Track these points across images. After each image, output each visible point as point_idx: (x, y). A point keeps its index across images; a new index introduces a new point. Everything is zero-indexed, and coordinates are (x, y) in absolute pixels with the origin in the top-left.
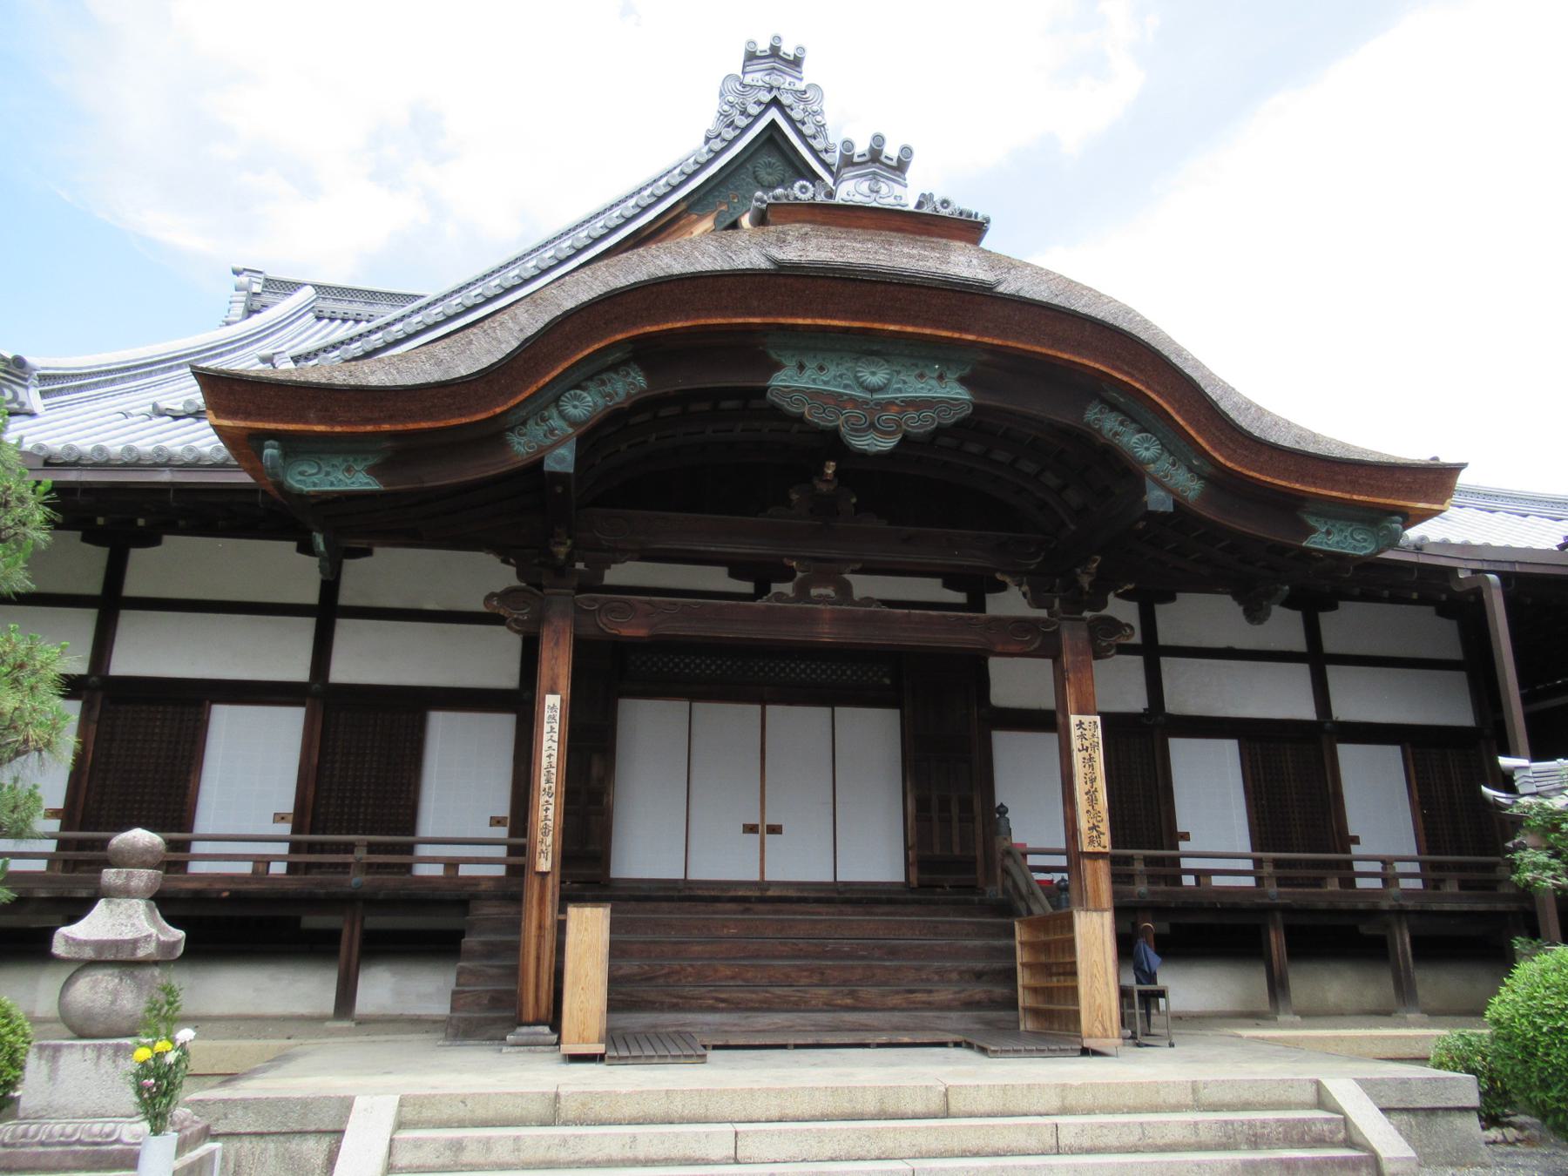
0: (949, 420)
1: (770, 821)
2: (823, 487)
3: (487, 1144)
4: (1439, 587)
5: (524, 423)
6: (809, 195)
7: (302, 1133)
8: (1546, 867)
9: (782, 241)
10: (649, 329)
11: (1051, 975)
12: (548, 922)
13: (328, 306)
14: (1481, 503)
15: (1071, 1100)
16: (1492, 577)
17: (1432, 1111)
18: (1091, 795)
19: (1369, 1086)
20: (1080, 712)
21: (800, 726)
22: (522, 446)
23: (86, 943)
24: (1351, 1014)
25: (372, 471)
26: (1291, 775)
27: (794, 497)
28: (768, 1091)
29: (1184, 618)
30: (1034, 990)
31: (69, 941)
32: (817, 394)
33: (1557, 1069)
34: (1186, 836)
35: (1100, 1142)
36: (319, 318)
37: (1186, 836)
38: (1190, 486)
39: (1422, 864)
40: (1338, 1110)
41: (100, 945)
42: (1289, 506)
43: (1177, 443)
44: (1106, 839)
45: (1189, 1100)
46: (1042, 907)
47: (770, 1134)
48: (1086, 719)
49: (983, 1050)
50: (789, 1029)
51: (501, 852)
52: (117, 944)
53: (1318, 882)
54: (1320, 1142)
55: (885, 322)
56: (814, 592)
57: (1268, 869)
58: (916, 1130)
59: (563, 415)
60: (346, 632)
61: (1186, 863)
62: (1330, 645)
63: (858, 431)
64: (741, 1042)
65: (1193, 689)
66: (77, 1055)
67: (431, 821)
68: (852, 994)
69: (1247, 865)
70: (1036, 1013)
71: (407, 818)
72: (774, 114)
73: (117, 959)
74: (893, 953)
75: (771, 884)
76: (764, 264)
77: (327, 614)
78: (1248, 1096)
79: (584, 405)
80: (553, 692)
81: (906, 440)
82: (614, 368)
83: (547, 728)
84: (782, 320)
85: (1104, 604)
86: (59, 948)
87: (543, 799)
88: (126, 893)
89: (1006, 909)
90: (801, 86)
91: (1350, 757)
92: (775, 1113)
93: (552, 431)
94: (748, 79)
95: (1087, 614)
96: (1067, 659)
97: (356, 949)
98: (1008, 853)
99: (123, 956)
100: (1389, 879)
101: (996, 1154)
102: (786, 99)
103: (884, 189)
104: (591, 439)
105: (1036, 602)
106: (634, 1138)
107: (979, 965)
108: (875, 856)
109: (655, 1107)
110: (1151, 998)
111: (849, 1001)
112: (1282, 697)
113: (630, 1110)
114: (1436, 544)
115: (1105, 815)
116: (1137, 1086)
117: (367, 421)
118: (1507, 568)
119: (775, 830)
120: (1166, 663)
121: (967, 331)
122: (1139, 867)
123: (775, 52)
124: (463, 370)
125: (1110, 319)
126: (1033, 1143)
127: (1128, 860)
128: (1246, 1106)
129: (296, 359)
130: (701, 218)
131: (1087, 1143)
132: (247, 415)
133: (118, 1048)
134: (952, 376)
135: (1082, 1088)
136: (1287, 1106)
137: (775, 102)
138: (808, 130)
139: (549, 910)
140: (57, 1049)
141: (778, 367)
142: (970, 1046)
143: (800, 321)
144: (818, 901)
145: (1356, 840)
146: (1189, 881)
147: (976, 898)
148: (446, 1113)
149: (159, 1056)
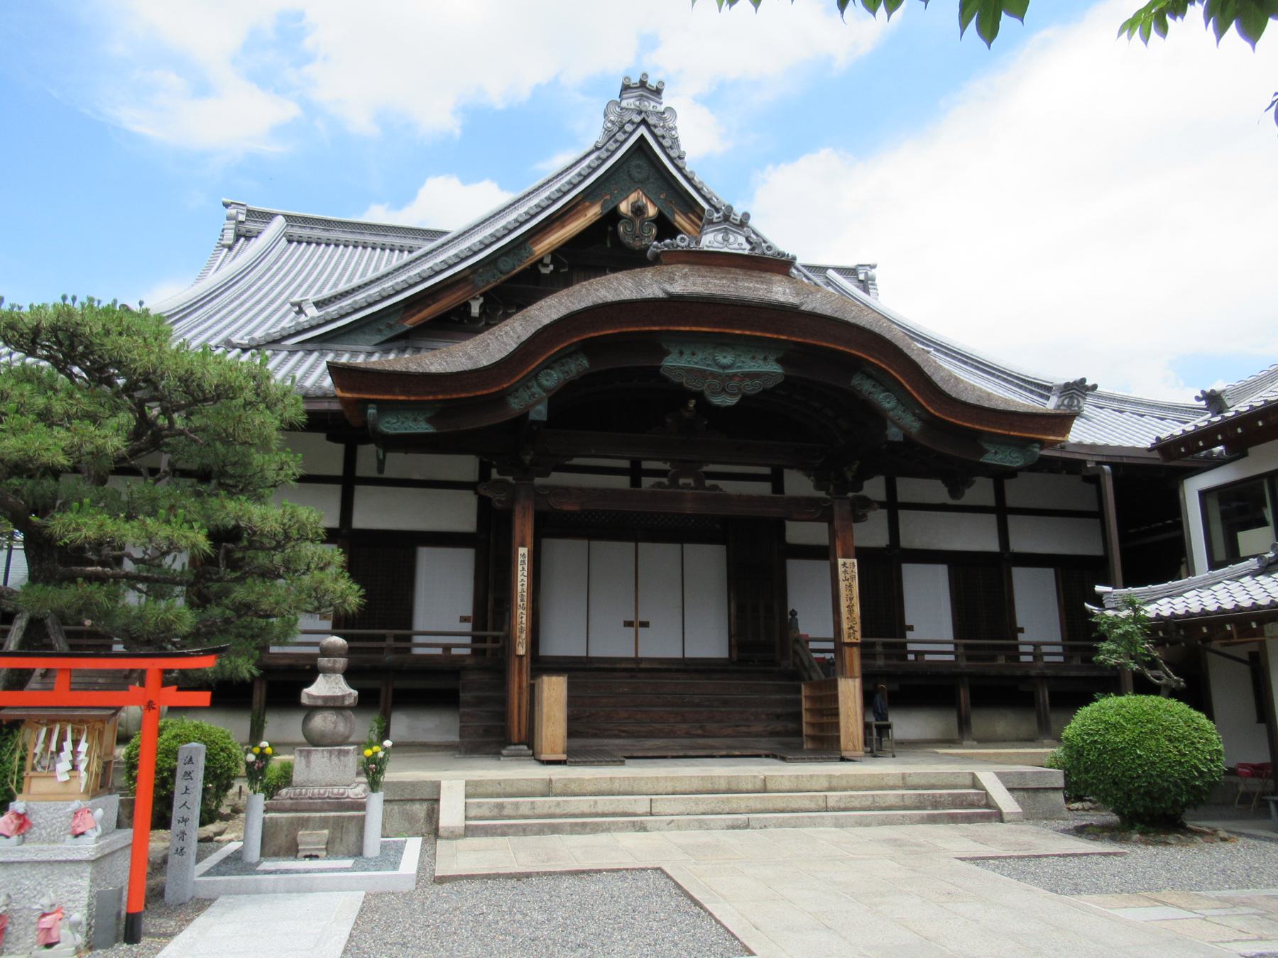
0: (770, 385)
1: (641, 618)
2: (687, 415)
3: (517, 805)
4: (1076, 467)
5: (517, 391)
6: (685, 244)
7: (412, 800)
8: (1115, 651)
9: (672, 280)
10: (593, 335)
11: (823, 716)
12: (525, 684)
13: (296, 231)
14: (1116, 405)
15: (834, 783)
16: (1106, 467)
17: (1037, 790)
18: (850, 608)
19: (1000, 776)
20: (844, 557)
21: (660, 555)
22: (515, 405)
23: (318, 697)
24: (1011, 741)
25: (429, 421)
26: (981, 590)
27: (669, 420)
28: (666, 778)
29: (909, 489)
30: (812, 725)
31: (309, 696)
32: (690, 371)
33: (1092, 762)
34: (911, 628)
35: (849, 805)
36: (290, 242)
37: (911, 628)
38: (914, 426)
39: (1064, 647)
40: (983, 789)
41: (326, 698)
42: (973, 438)
43: (906, 400)
44: (858, 635)
45: (900, 783)
46: (818, 675)
47: (670, 800)
48: (848, 561)
49: (783, 759)
50: (666, 748)
51: (468, 640)
52: (334, 698)
53: (993, 658)
54: (972, 805)
55: (732, 327)
56: (682, 481)
57: (961, 650)
58: (749, 799)
59: (540, 385)
60: (362, 495)
61: (911, 647)
62: (1011, 500)
63: (715, 393)
64: (640, 754)
65: (921, 532)
66: (320, 755)
67: (422, 621)
68: (701, 727)
69: (951, 648)
70: (813, 738)
71: (406, 618)
72: (643, 130)
73: (332, 705)
74: (725, 703)
75: (643, 660)
76: (661, 295)
77: (348, 483)
78: (933, 781)
79: (552, 379)
80: (523, 545)
81: (745, 398)
82: (570, 355)
83: (520, 568)
84: (671, 328)
85: (861, 488)
86: (304, 700)
87: (520, 611)
88: (332, 671)
89: (796, 676)
90: (661, 108)
91: (1020, 575)
92: (670, 789)
93: (533, 395)
94: (624, 104)
95: (850, 495)
96: (837, 523)
97: (390, 701)
98: (797, 641)
99: (338, 704)
100: (1037, 656)
101: (793, 811)
102: (652, 120)
103: (732, 238)
104: (557, 399)
105: (818, 487)
106: (596, 802)
107: (779, 710)
108: (709, 640)
109: (605, 786)
110: (884, 729)
111: (700, 732)
112: (976, 537)
113: (590, 788)
114: (1074, 445)
115: (858, 620)
116: (871, 776)
117: (430, 393)
118: (1118, 460)
119: (645, 624)
120: (902, 514)
121: (782, 334)
122: (879, 649)
123: (643, 84)
124: (485, 362)
125: (868, 326)
126: (813, 805)
127: (873, 645)
128: (932, 787)
129: (319, 304)
130: (592, 204)
131: (842, 805)
132: (359, 391)
133: (340, 751)
134: (771, 358)
135: (840, 777)
136: (955, 787)
137: (644, 122)
138: (666, 143)
139: (525, 678)
140: (309, 752)
141: (667, 353)
142: (775, 757)
143: (682, 329)
144: (678, 671)
145: (1021, 630)
146: (911, 657)
147: (776, 669)
148: (490, 790)
149: (376, 753)
